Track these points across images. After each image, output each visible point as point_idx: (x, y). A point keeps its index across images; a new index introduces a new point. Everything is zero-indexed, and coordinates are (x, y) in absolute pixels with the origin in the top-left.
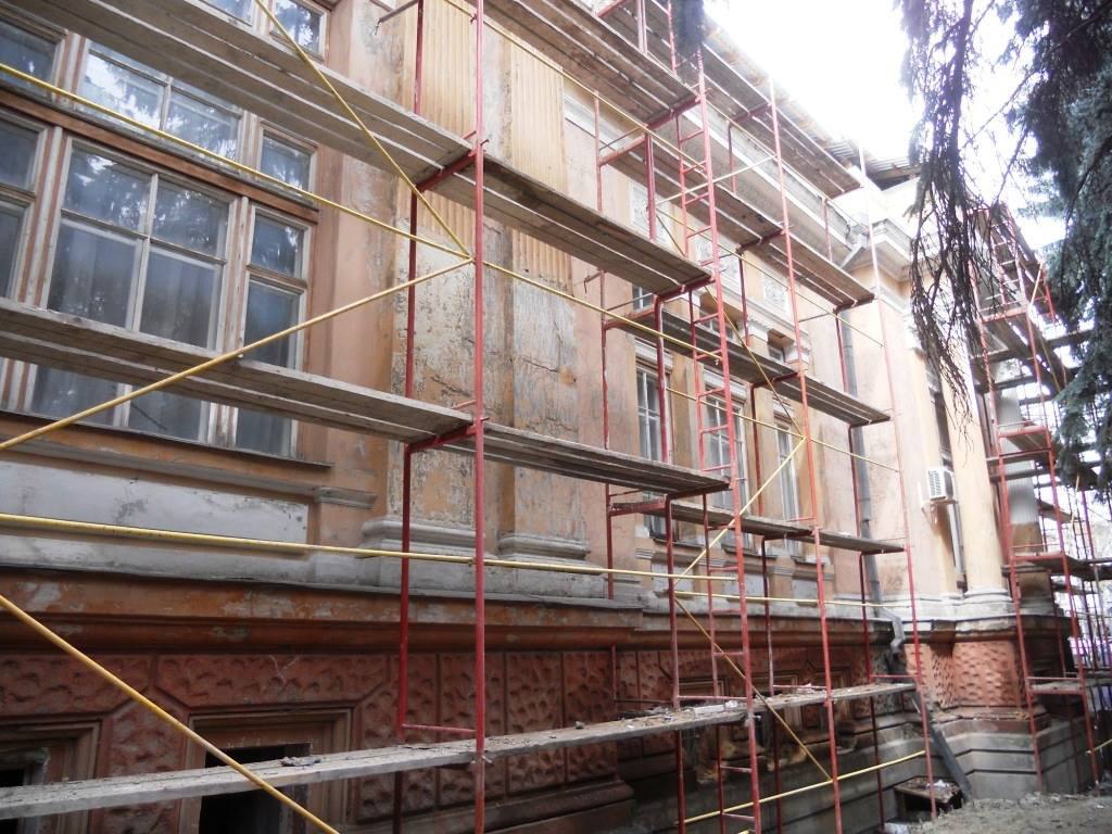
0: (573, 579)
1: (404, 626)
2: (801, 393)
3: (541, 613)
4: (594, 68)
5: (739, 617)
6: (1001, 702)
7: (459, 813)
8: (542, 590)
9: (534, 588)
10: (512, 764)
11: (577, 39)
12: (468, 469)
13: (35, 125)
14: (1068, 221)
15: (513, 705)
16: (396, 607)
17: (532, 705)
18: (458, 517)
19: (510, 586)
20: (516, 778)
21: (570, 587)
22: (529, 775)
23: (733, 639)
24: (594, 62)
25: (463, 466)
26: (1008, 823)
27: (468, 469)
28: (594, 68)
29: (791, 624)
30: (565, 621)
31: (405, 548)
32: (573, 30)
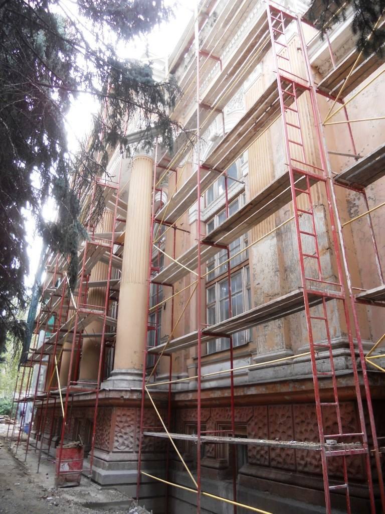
0: (324, 362)
1: (233, 397)
2: (184, 268)
3: (291, 385)
4: (263, 123)
5: (311, 379)
6: (20, 438)
7: (276, 471)
8: (307, 372)
9: (302, 372)
10: (298, 457)
11: (243, 134)
12: (281, 325)
13: (212, 286)
14: (90, 60)
15: (298, 429)
16: (229, 391)
17: (306, 430)
18: (279, 347)
19: (291, 373)
20: (300, 464)
21: (322, 367)
22: (306, 465)
23: (329, 394)
24: (258, 124)
25: (279, 325)
26: (38, 498)
27: (281, 325)
28: (263, 123)
29: (297, 385)
30: (304, 387)
31: (232, 372)
32: (240, 135)
